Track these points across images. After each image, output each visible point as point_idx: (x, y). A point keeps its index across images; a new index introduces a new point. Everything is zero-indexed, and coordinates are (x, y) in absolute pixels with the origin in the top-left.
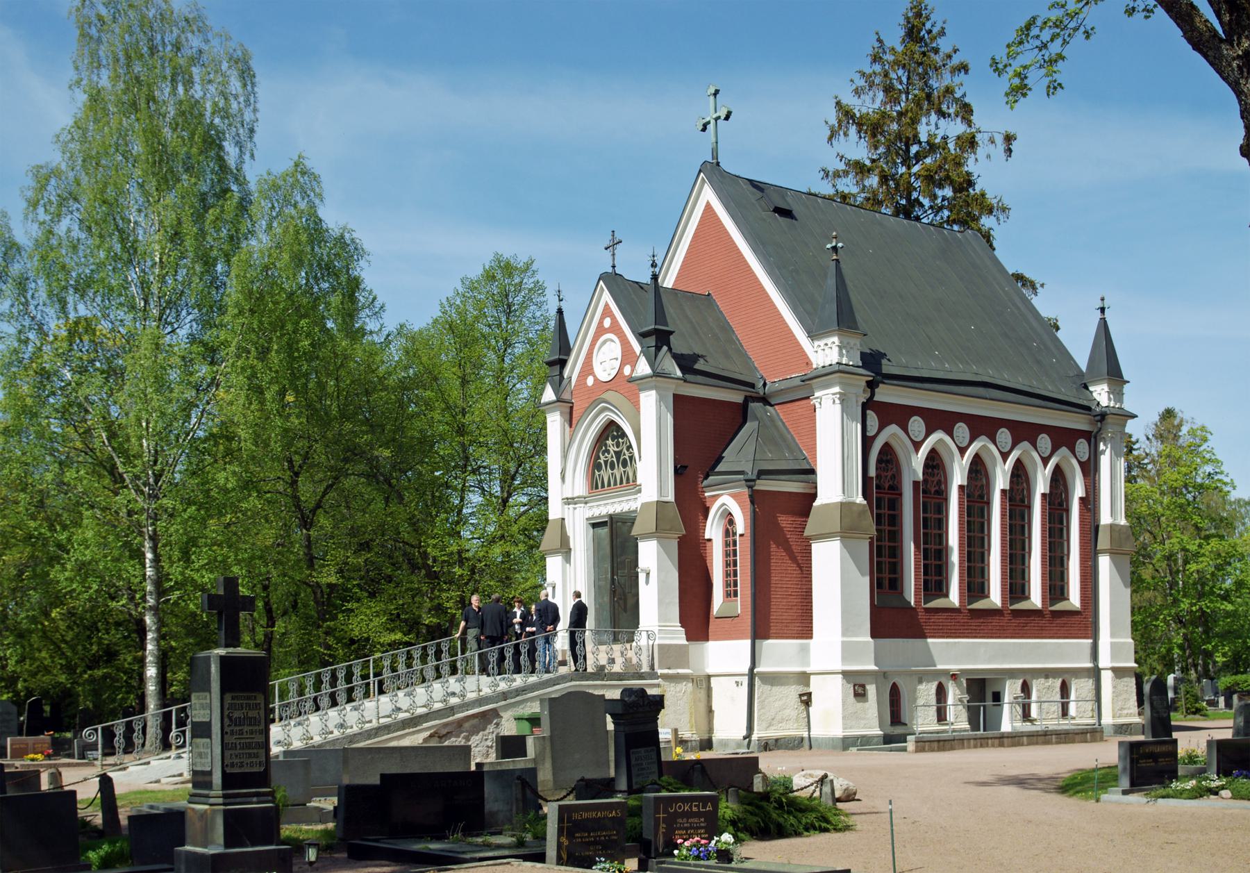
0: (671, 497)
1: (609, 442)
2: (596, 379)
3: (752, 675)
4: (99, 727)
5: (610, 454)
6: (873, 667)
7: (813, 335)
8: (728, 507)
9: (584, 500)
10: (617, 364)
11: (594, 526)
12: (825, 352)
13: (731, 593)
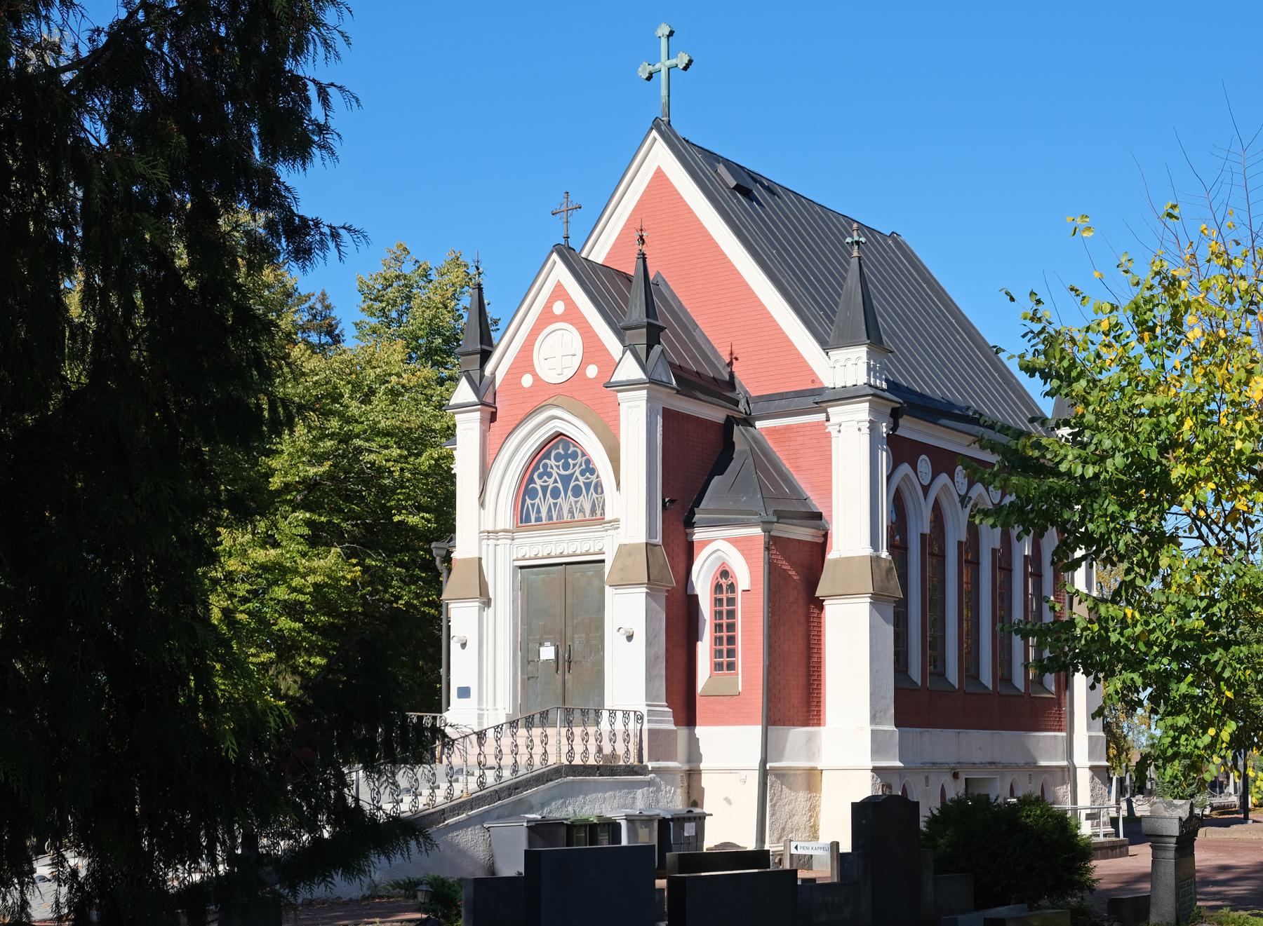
0: (658, 540)
1: (552, 462)
3: (764, 773)
4: (772, 868)
5: (558, 475)
6: (898, 764)
7: (826, 345)
8: (727, 555)
9: (510, 533)
10: (576, 362)
12: (849, 366)
13: (724, 663)
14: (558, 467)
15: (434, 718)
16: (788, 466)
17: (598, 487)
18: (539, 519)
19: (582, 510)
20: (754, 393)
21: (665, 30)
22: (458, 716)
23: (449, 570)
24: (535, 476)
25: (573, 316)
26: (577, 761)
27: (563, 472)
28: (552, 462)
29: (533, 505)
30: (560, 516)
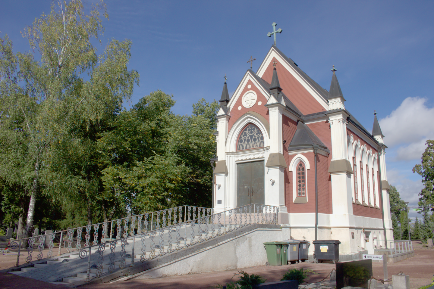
1: (247, 131)
2: (243, 107)
3: (316, 227)
5: (250, 136)
11: (237, 164)
14: (249, 133)
15: (210, 210)
16: (316, 134)
17: (262, 138)
18: (243, 149)
19: (257, 146)
20: (304, 114)
21: (274, 24)
22: (217, 209)
23: (215, 166)
24: (242, 136)
25: (254, 88)
26: (260, 223)
27: (250, 134)
28: (247, 131)
29: (241, 145)
30: (250, 147)
